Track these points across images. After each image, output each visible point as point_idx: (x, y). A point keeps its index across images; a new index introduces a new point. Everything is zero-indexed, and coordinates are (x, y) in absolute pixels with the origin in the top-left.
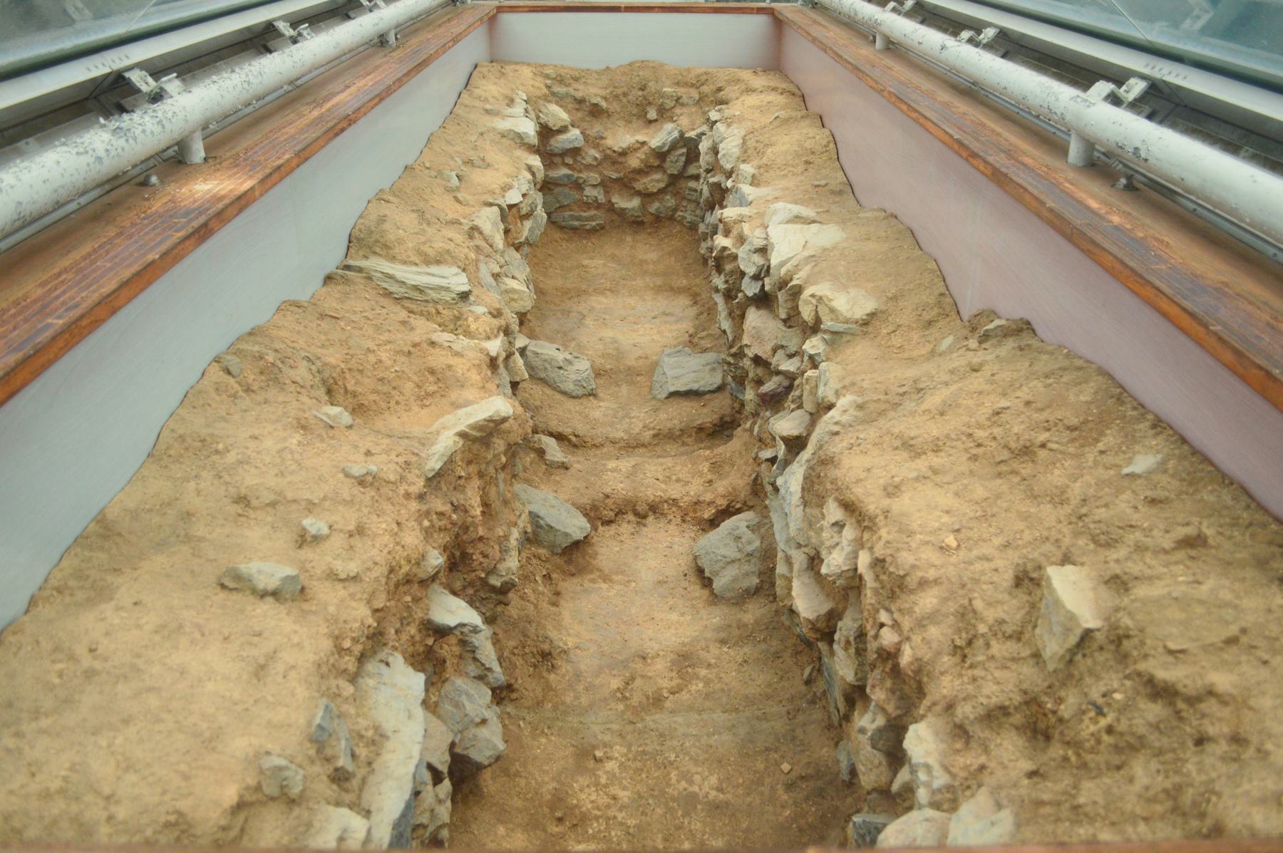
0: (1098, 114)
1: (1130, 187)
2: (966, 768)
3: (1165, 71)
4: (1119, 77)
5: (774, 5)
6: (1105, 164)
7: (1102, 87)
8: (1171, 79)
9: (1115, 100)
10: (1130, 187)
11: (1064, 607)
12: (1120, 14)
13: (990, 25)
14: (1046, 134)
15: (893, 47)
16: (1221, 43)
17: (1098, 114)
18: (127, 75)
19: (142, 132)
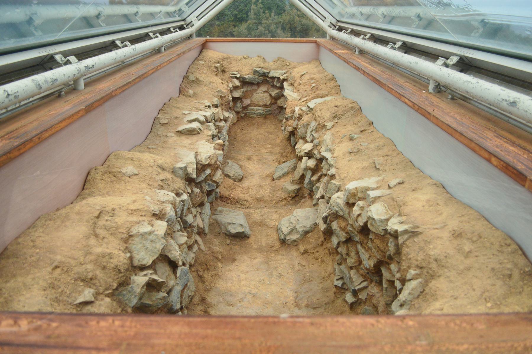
0: (435, 69)
1: (452, 99)
2: (221, 175)
3: (465, 52)
4: (447, 56)
5: (317, 39)
6: (441, 89)
7: (441, 61)
8: (471, 56)
9: (446, 65)
10: (452, 99)
11: (21, 23)
12: (448, 32)
13: (399, 41)
14: (419, 80)
15: (362, 52)
16: (71, 32)
17: (435, 69)
18: (77, 61)
19: (87, 76)
